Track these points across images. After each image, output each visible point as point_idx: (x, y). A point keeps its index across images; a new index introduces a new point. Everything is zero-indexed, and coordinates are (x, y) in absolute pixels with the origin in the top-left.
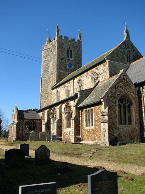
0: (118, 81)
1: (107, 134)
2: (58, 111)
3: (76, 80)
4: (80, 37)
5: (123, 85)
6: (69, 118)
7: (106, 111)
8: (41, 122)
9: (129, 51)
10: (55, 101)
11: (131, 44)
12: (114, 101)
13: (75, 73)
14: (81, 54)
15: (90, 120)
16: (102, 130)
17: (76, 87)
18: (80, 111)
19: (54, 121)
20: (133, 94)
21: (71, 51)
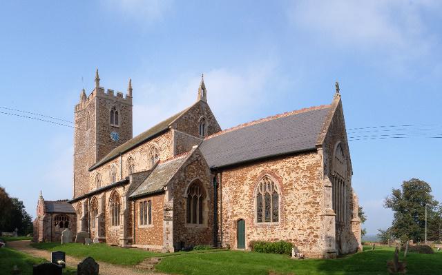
0: (189, 162)
1: (171, 237)
2: (100, 201)
3: (125, 157)
4: (131, 90)
6: (116, 210)
7: (171, 204)
8: (76, 216)
9: (203, 119)
10: (95, 189)
11: (208, 108)
13: (126, 146)
14: (131, 118)
15: (147, 216)
16: (165, 231)
17: (124, 168)
18: (133, 203)
19: (94, 215)
21: (117, 113)
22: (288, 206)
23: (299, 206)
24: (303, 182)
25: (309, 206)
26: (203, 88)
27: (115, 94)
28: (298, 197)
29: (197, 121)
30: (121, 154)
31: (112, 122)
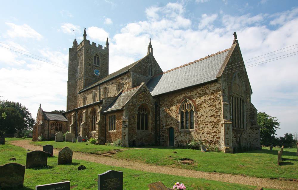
0: (139, 92)
5: (142, 96)
9: (151, 65)
12: (134, 109)
20: (151, 104)
21: (98, 58)
22: (200, 118)
23: (207, 118)
24: (209, 102)
25: (213, 117)
26: (150, 46)
27: (97, 46)
28: (206, 112)
29: (147, 70)
30: (100, 85)
31: (95, 63)
